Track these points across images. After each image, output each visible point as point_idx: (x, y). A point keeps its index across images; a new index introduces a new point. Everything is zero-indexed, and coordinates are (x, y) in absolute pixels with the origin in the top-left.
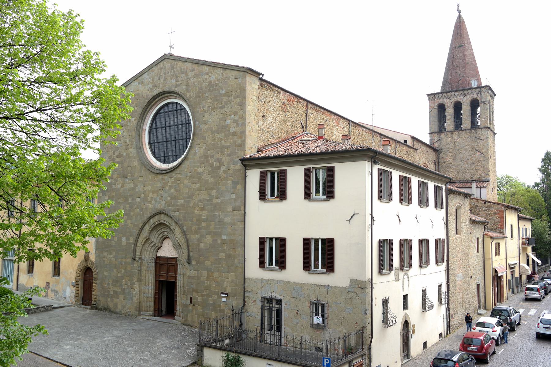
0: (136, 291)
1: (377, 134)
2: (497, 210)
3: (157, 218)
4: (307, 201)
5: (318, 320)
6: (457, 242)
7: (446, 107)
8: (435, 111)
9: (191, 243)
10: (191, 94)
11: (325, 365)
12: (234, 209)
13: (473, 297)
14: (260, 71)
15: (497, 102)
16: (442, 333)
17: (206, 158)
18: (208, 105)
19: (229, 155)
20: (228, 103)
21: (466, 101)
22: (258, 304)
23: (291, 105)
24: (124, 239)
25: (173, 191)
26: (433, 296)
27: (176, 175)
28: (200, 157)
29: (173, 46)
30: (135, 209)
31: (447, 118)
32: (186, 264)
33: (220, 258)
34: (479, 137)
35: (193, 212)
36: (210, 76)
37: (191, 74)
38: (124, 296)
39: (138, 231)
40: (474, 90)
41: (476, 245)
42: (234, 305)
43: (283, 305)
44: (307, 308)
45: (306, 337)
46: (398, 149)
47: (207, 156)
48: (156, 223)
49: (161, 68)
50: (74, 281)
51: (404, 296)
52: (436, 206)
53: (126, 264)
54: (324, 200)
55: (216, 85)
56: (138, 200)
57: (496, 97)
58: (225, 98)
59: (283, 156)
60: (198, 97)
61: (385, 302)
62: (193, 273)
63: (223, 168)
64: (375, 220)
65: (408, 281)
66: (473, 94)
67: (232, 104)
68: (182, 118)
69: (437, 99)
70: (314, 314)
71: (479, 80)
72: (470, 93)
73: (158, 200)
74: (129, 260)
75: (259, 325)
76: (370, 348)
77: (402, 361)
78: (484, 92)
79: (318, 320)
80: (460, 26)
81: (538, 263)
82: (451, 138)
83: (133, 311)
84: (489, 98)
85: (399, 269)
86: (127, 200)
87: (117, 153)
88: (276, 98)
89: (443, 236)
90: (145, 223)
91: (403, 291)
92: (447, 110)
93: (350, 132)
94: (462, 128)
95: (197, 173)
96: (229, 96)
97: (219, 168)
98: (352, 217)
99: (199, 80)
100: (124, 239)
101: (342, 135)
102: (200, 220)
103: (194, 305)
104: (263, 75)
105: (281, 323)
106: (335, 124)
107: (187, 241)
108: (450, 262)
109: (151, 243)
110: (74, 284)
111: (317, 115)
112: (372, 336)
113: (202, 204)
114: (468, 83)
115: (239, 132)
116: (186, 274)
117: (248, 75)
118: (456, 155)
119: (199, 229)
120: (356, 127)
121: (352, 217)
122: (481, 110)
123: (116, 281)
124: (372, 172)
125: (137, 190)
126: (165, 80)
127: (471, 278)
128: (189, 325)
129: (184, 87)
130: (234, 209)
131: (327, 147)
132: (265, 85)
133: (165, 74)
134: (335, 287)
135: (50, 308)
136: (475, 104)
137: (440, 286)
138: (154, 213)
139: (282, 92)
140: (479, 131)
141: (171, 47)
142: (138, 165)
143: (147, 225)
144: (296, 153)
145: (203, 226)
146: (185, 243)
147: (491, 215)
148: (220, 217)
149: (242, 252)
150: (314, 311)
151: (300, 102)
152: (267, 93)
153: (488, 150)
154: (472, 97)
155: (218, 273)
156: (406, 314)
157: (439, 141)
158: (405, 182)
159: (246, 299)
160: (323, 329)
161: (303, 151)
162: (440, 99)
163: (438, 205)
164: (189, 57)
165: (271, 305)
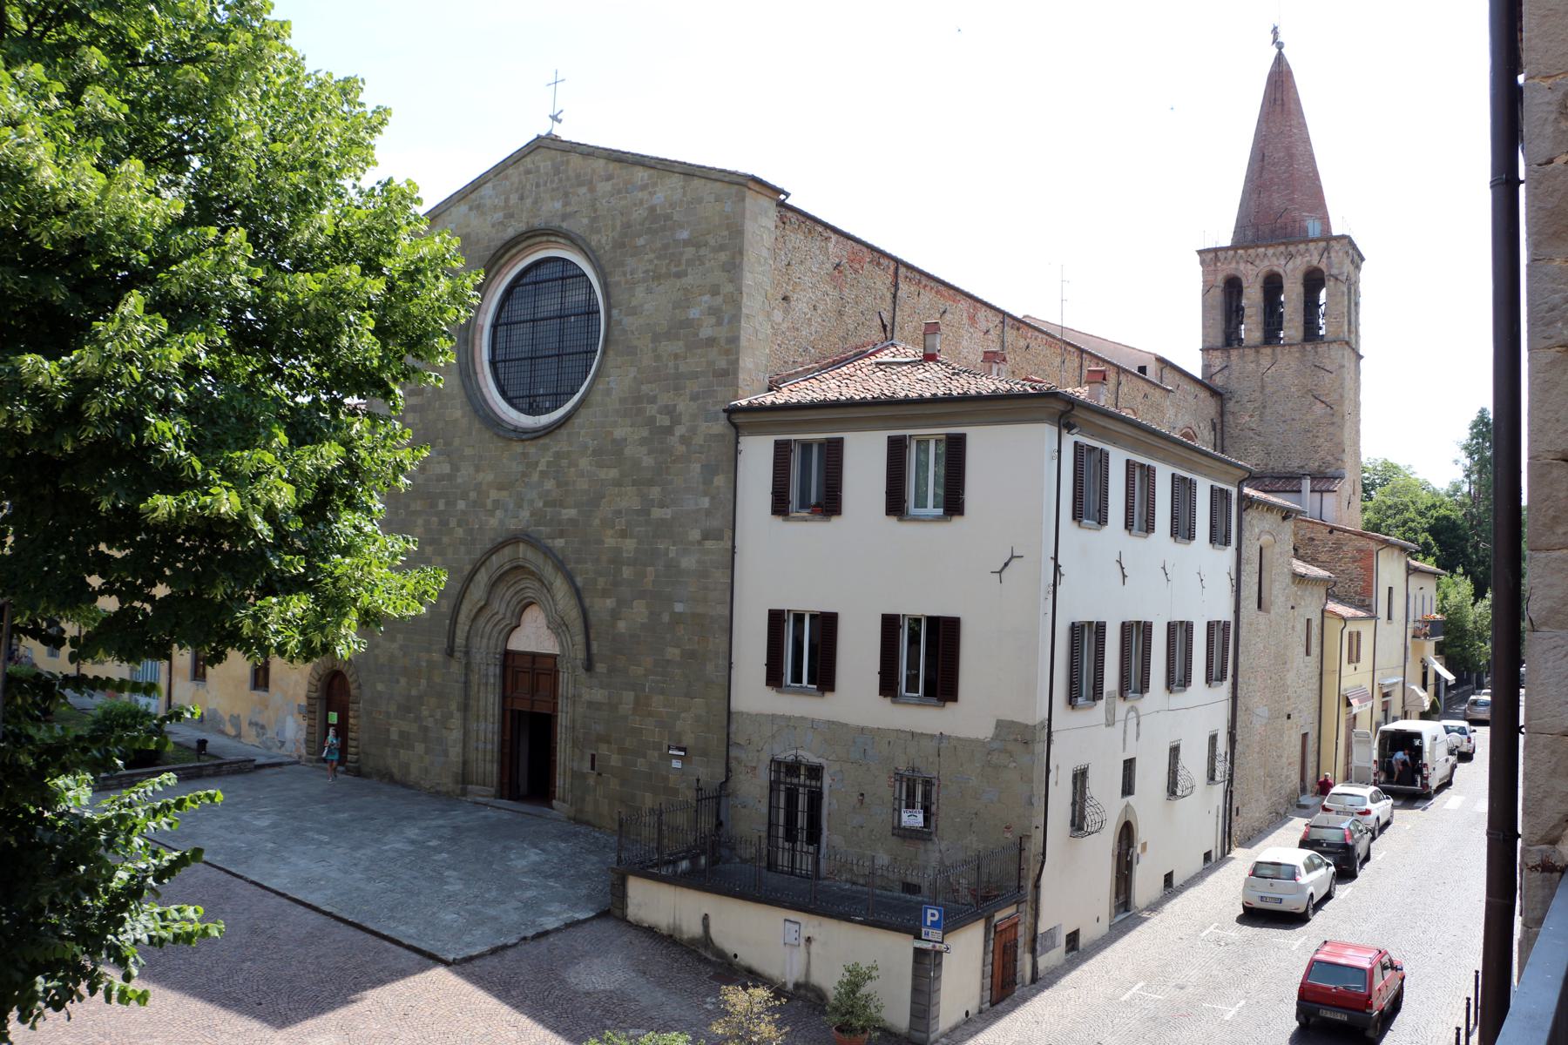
0: (455, 735)
1: (1073, 350)
2: (1360, 551)
4: (893, 520)
5: (913, 819)
6: (1259, 630)
8: (1218, 294)
9: (593, 619)
10: (602, 240)
11: (929, 923)
12: (706, 536)
13: (1290, 764)
14: (779, 186)
15: (1367, 279)
16: (1210, 851)
17: (635, 404)
18: (644, 269)
19: (694, 398)
20: (697, 263)
22: (764, 777)
23: (856, 271)
25: (549, 485)
26: (1194, 763)
27: (560, 443)
28: (622, 401)
29: (559, 117)
31: (1246, 311)
32: (581, 672)
33: (668, 661)
34: (1322, 365)
35: (602, 542)
36: (652, 194)
39: (460, 585)
40: (1312, 246)
41: (1304, 638)
42: (703, 778)
44: (883, 789)
45: (883, 859)
46: (1124, 389)
47: (638, 399)
48: (507, 567)
50: (304, 702)
51: (1125, 762)
52: (1212, 540)
54: (937, 519)
55: (668, 217)
56: (461, 505)
57: (1364, 266)
58: (690, 252)
59: (836, 405)
60: (619, 245)
61: (1080, 777)
62: (599, 695)
63: (680, 430)
64: (1062, 572)
65: (1138, 724)
66: (1311, 255)
68: (576, 297)
69: (1223, 264)
70: (903, 803)
71: (1325, 220)
72: (1302, 251)
74: (437, 657)
75: (765, 828)
76: (1037, 886)
77: (1111, 917)
78: (1337, 252)
79: (913, 819)
80: (1280, 84)
81: (1447, 681)
82: (1253, 365)
83: (448, 783)
84: (1348, 267)
85: (1117, 694)
86: (433, 505)
88: (818, 252)
89: (1226, 614)
91: (1124, 748)
92: (1244, 290)
93: (1003, 342)
94: (1281, 339)
95: (614, 441)
96: (698, 246)
97: (669, 430)
98: (1006, 565)
99: (623, 202)
101: (985, 352)
102: (617, 560)
103: (599, 774)
104: (788, 195)
105: (820, 825)
106: (965, 320)
108: (1240, 680)
111: (921, 296)
112: (1044, 858)
113: (623, 520)
114: (1298, 225)
116: (580, 696)
117: (749, 194)
118: (1264, 407)
120: (1018, 329)
121: (1006, 565)
122: (1328, 295)
123: (408, 708)
124: (1059, 451)
125: (459, 480)
126: (535, 202)
128: (588, 823)
129: (585, 221)
130: (706, 536)
131: (949, 385)
132: (793, 220)
133: (538, 185)
134: (958, 739)
135: (251, 765)
136: (1313, 281)
137: (1213, 739)
138: (500, 540)
139: (834, 237)
140: (1322, 348)
141: (555, 118)
142: (463, 417)
143: (483, 570)
144: (869, 397)
145: (625, 576)
147: (1343, 561)
148: (671, 555)
149: (724, 647)
150: (904, 797)
151: (879, 264)
152: (796, 239)
153: (1342, 396)
154: (1308, 261)
155: (661, 697)
156: (1128, 805)
157: (1226, 372)
158: (1140, 478)
159: (733, 764)
160: (924, 840)
161: (886, 392)
162: (1230, 263)
163: (1218, 536)
164: (601, 145)
165: (795, 781)
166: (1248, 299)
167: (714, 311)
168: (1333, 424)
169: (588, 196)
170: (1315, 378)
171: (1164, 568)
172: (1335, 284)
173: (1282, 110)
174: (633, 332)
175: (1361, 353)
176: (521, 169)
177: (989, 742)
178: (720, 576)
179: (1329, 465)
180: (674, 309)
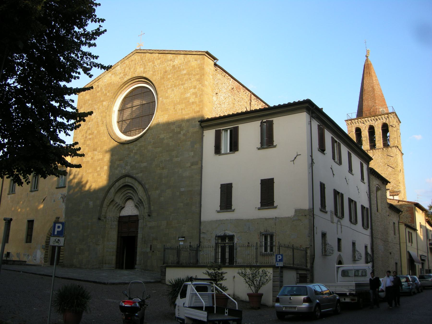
3: (122, 181)
7: (362, 130)
12: (192, 164)
21: (378, 124)
37: (157, 62)
40: (383, 116)
43: (236, 240)
49: (132, 61)
55: (179, 68)
58: (187, 77)
60: (162, 78)
61: (324, 235)
65: (341, 228)
67: (192, 80)
78: (391, 118)
86: (96, 169)
87: (89, 132)
90: (111, 187)
91: (337, 234)
92: (362, 132)
97: (179, 133)
98: (295, 158)
100: (91, 203)
103: (153, 252)
107: (149, 198)
109: (116, 204)
121: (295, 158)
127: (390, 253)
134: (282, 218)
137: (366, 247)
138: (119, 177)
143: (113, 188)
145: (163, 182)
150: (263, 241)
166: (363, 135)
167: (195, 94)
168: (395, 174)
169: (152, 65)
170: (388, 159)
171: (346, 179)
172: (392, 128)
173: (370, 75)
174: (167, 104)
175: (403, 152)
176: (130, 60)
177: (293, 217)
178: (200, 162)
179: (395, 188)
180: (181, 95)
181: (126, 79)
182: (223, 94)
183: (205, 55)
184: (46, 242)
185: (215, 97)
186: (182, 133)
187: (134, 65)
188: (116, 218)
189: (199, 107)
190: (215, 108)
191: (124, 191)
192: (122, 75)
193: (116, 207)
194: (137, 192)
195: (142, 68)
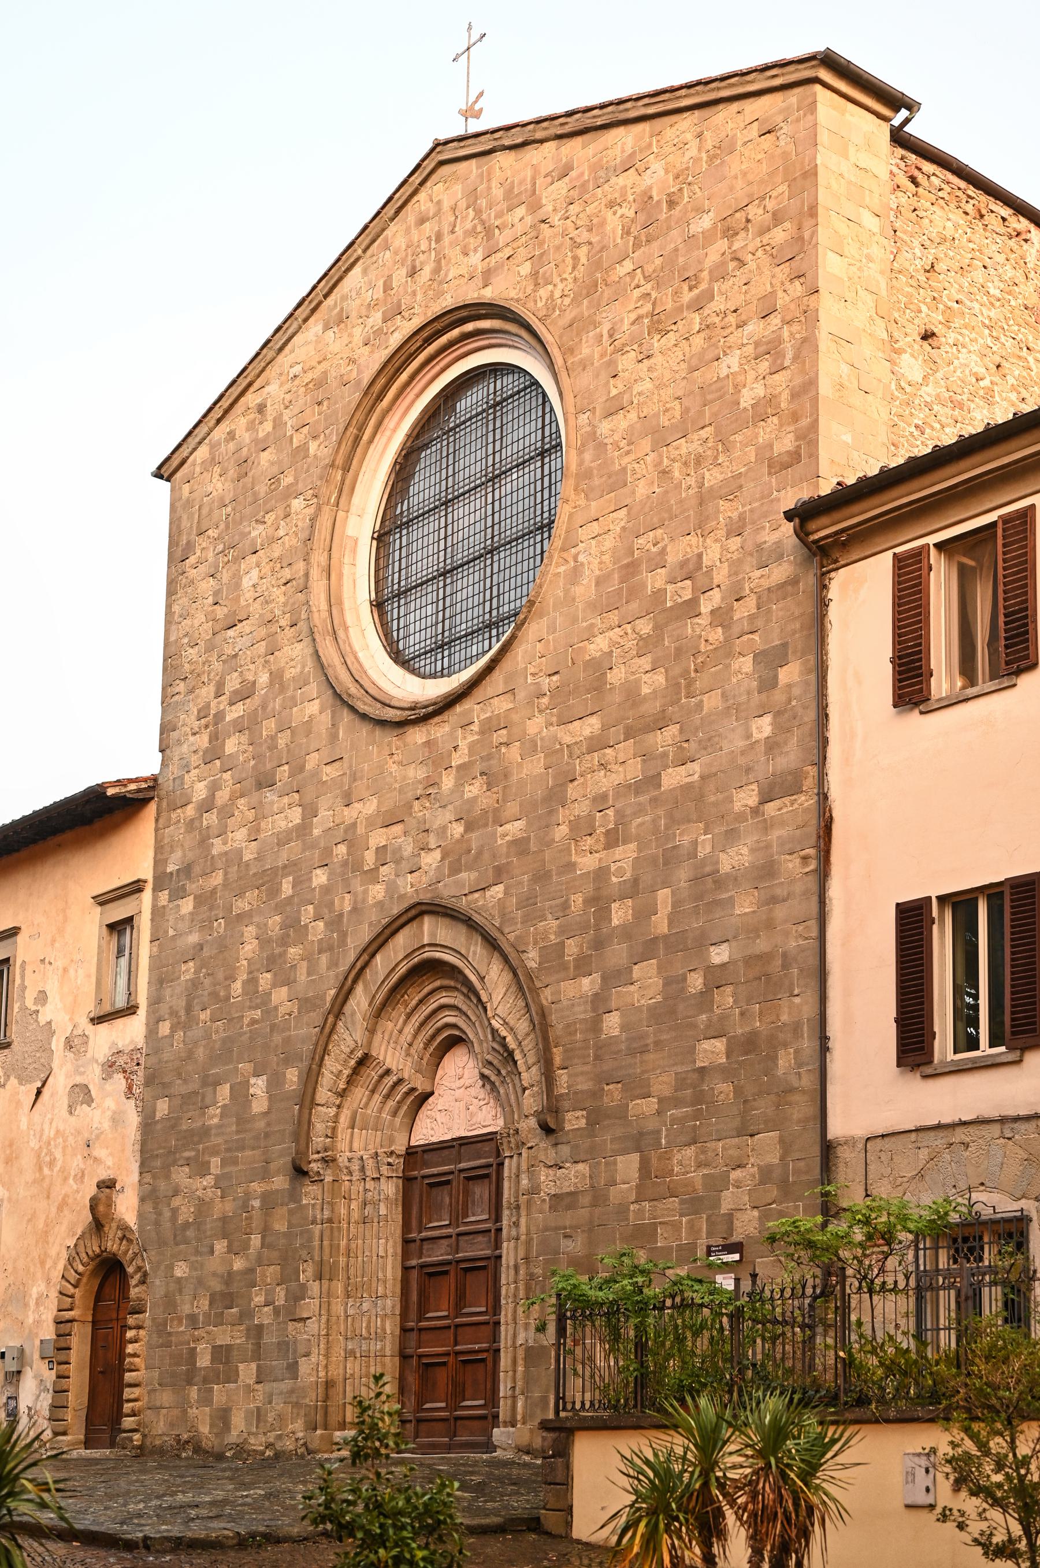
3: (402, 942)
19: (736, 530)
20: (732, 265)
24: (259, 1086)
25: (474, 789)
30: (306, 926)
35: (571, 866)
38: (259, 1367)
47: (630, 569)
48: (402, 970)
53: (269, 1202)
56: (320, 877)
73: (408, 850)
74: (280, 1182)
87: (233, 683)
97: (690, 608)
100: (259, 1086)
109: (382, 1077)
110: (50, 1351)
115: (785, 396)
119: (599, 944)
125: (316, 832)
143: (359, 989)
145: (615, 922)
146: (532, 1036)
181: (395, 340)
182: (973, 336)
183: (816, 80)
184: (58, 1322)
185: (912, 356)
186: (705, 608)
187: (433, 245)
188: (390, 1160)
189: (792, 428)
190: (917, 427)
191: (421, 1001)
192: (376, 317)
193: (387, 1096)
194: (484, 999)
195: (475, 250)
